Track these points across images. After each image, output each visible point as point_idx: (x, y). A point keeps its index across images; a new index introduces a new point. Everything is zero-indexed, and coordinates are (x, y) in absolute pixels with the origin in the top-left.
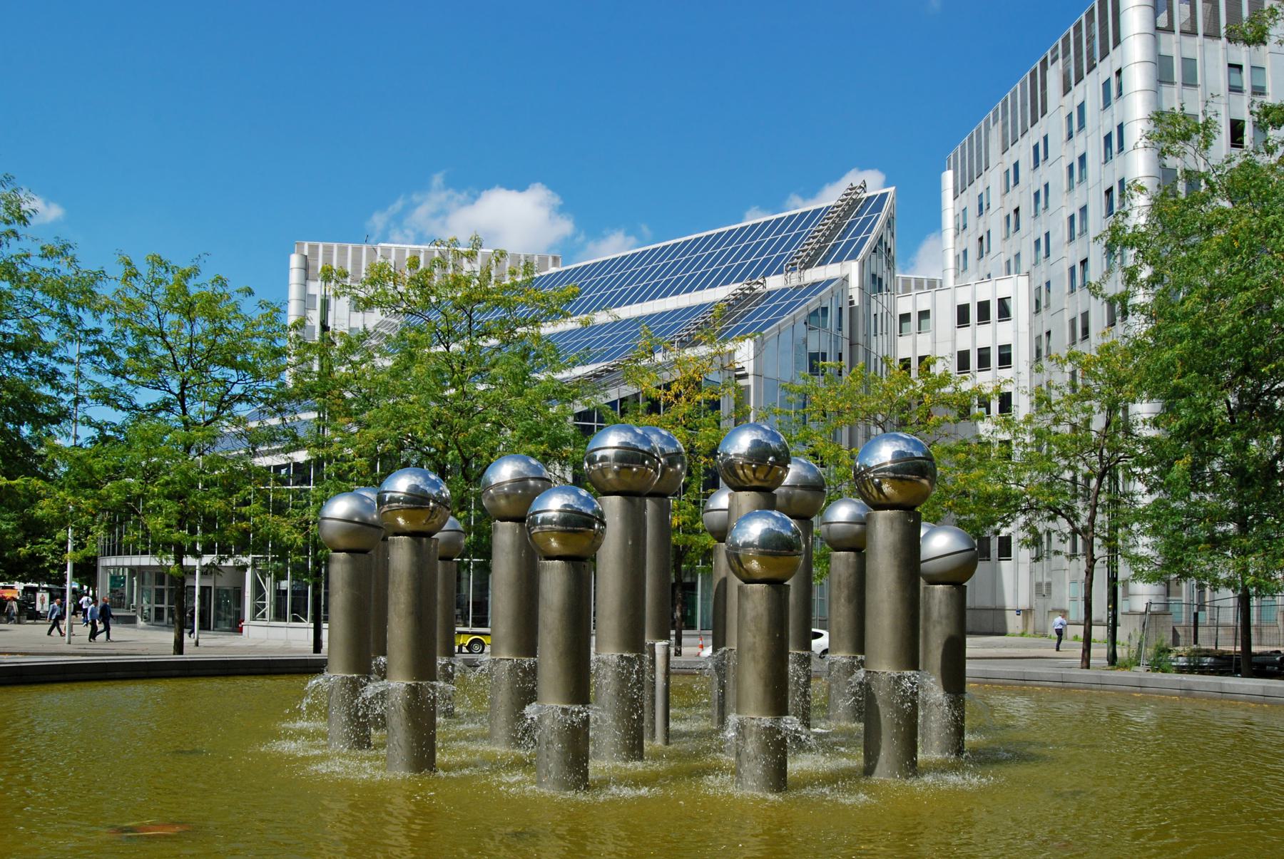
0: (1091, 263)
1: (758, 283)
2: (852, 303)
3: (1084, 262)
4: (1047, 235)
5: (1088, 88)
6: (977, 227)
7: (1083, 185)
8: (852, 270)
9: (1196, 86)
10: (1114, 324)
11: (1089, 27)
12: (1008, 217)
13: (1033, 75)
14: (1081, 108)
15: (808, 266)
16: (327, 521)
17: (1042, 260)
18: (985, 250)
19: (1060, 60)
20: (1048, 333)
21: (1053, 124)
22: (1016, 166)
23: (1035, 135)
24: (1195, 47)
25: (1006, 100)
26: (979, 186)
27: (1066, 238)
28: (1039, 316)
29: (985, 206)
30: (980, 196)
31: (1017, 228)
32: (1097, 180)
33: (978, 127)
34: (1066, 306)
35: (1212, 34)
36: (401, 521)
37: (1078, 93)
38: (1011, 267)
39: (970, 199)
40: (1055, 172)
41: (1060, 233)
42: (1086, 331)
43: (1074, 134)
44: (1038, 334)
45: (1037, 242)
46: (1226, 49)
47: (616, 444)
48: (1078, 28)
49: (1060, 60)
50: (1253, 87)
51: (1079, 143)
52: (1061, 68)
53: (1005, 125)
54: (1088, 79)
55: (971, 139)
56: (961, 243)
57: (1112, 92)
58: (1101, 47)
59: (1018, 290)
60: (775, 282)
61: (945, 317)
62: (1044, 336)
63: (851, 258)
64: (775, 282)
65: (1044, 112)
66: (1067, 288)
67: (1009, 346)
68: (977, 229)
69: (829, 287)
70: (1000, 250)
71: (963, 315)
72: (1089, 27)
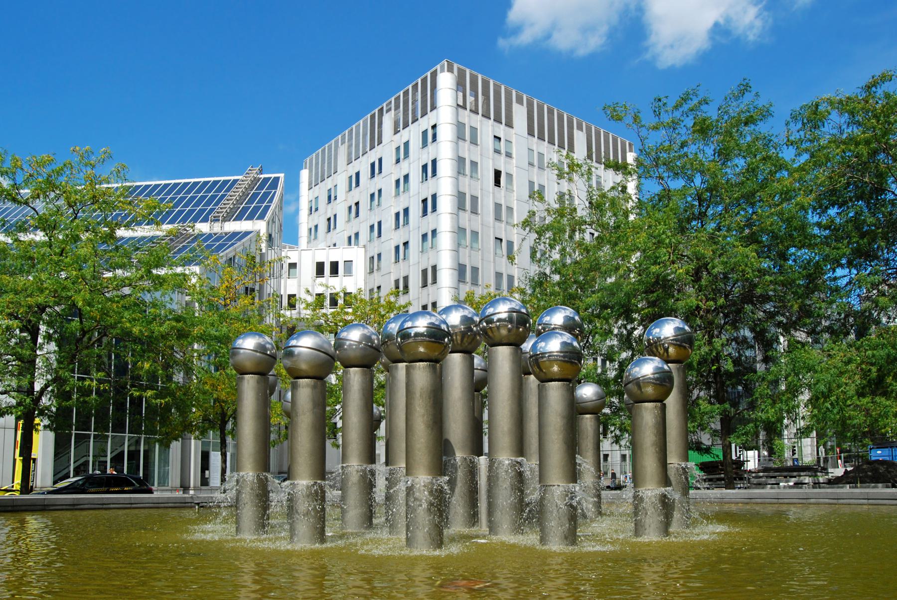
0: (411, 244)
1: (189, 226)
2: (261, 250)
3: (406, 244)
4: (380, 223)
5: (413, 134)
6: (326, 211)
7: (406, 194)
8: (261, 226)
9: (477, 144)
10: (370, 290)
11: (414, 94)
12: (350, 208)
13: (373, 117)
14: (407, 144)
15: (226, 219)
16: (242, 351)
17: (376, 239)
18: (332, 227)
19: (393, 111)
20: (379, 288)
21: (386, 151)
22: (358, 174)
23: (373, 156)
24: (477, 120)
25: (352, 130)
26: (329, 183)
27: (393, 227)
28: (372, 275)
29: (333, 198)
30: (330, 190)
31: (357, 215)
32: (417, 192)
33: (329, 144)
34: (392, 271)
35: (486, 116)
36: (422, 349)
37: (404, 135)
38: (353, 239)
39: (321, 191)
40: (386, 182)
41: (389, 223)
42: (406, 287)
43: (401, 160)
44: (371, 287)
45: (372, 227)
46: (493, 126)
47: (507, 310)
48: (406, 93)
49: (393, 111)
50: (506, 152)
51: (404, 167)
52: (393, 116)
53: (350, 146)
54: (412, 127)
55: (323, 151)
56: (313, 220)
57: (430, 136)
58: (422, 109)
59: (358, 256)
60: (203, 227)
61: (307, 269)
62: (376, 290)
63: (261, 217)
64: (203, 227)
65: (380, 142)
66: (393, 260)
67: (294, 296)
68: (326, 212)
69: (249, 237)
70: (344, 228)
71: (320, 269)
72: (414, 94)
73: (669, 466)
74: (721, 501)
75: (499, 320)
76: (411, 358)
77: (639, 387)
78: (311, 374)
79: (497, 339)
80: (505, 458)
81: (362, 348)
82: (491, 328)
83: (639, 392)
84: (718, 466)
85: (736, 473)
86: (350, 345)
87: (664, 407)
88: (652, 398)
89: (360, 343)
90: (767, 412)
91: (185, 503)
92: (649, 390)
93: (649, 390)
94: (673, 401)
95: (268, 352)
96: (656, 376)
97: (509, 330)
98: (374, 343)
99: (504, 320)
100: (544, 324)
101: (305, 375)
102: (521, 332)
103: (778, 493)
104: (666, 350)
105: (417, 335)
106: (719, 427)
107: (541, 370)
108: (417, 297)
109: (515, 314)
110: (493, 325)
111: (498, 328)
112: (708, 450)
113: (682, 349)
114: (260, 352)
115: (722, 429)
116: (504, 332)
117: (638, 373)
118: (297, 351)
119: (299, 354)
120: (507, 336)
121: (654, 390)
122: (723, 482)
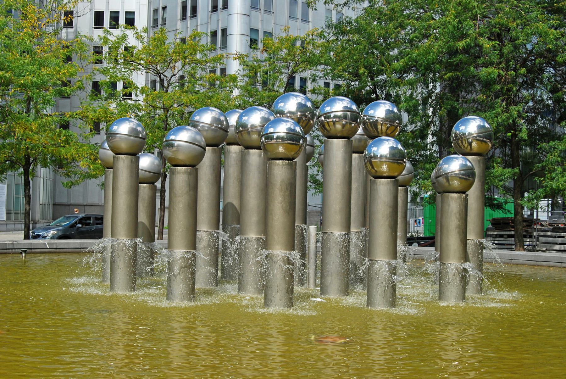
10: (154, 11)
20: (164, 8)
36: (281, 149)
44: (156, 7)
62: (160, 11)
73: (468, 241)
74: (509, 262)
75: (335, 117)
76: (273, 156)
77: (448, 180)
78: (188, 163)
79: (333, 132)
80: (337, 232)
81: (213, 130)
82: (328, 122)
83: (447, 184)
84: (509, 223)
85: (526, 231)
86: (203, 126)
87: (466, 200)
88: (458, 190)
89: (211, 125)
90: (558, 181)
91: (7, 249)
92: (456, 183)
93: (456, 183)
94: (474, 193)
95: (140, 136)
96: (462, 172)
97: (344, 126)
98: (223, 124)
99: (339, 117)
100: (369, 116)
101: (182, 163)
102: (353, 126)
103: (561, 257)
104: (470, 144)
105: (278, 138)
106: (512, 185)
107: (373, 168)
108: (205, 21)
109: (349, 113)
110: (331, 120)
111: (334, 123)
112: (499, 206)
113: (484, 143)
114: (133, 136)
115: (514, 188)
116: (339, 126)
117: (448, 169)
118: (176, 143)
119: (178, 146)
120: (342, 131)
121: (461, 183)
122: (513, 239)
